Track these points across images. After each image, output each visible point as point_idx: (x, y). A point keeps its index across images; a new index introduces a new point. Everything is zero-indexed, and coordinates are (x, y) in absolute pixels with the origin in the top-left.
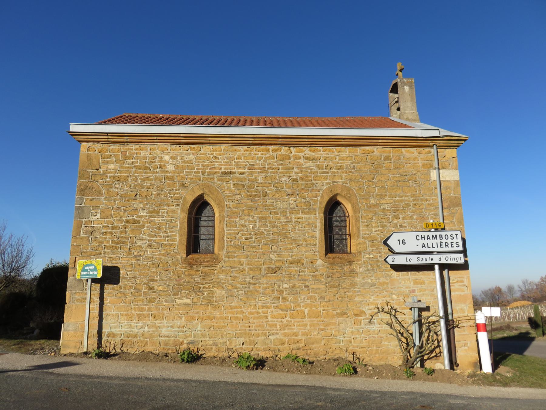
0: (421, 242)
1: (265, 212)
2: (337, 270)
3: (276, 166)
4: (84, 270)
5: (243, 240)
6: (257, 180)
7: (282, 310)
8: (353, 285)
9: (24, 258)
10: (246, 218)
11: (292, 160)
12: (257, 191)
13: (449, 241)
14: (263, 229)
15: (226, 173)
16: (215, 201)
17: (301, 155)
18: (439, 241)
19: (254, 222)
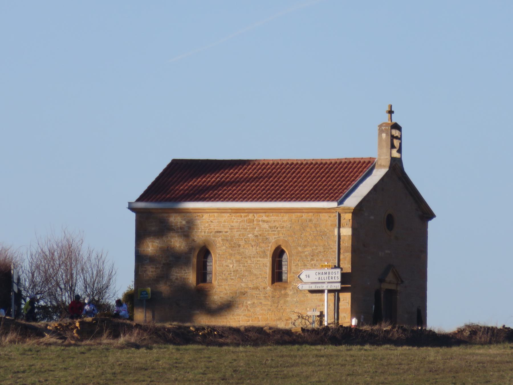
0: (318, 276)
1: (238, 257)
2: (277, 293)
3: (245, 227)
4: (141, 294)
5: (227, 275)
6: (235, 236)
7: (247, 317)
8: (285, 302)
9: (106, 278)
10: (229, 261)
11: (255, 223)
12: (235, 243)
13: (333, 276)
14: (238, 268)
15: (218, 232)
16: (287, 249)
17: (260, 219)
18: (328, 275)
19: (233, 263)
